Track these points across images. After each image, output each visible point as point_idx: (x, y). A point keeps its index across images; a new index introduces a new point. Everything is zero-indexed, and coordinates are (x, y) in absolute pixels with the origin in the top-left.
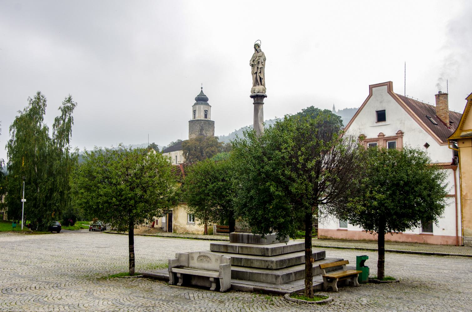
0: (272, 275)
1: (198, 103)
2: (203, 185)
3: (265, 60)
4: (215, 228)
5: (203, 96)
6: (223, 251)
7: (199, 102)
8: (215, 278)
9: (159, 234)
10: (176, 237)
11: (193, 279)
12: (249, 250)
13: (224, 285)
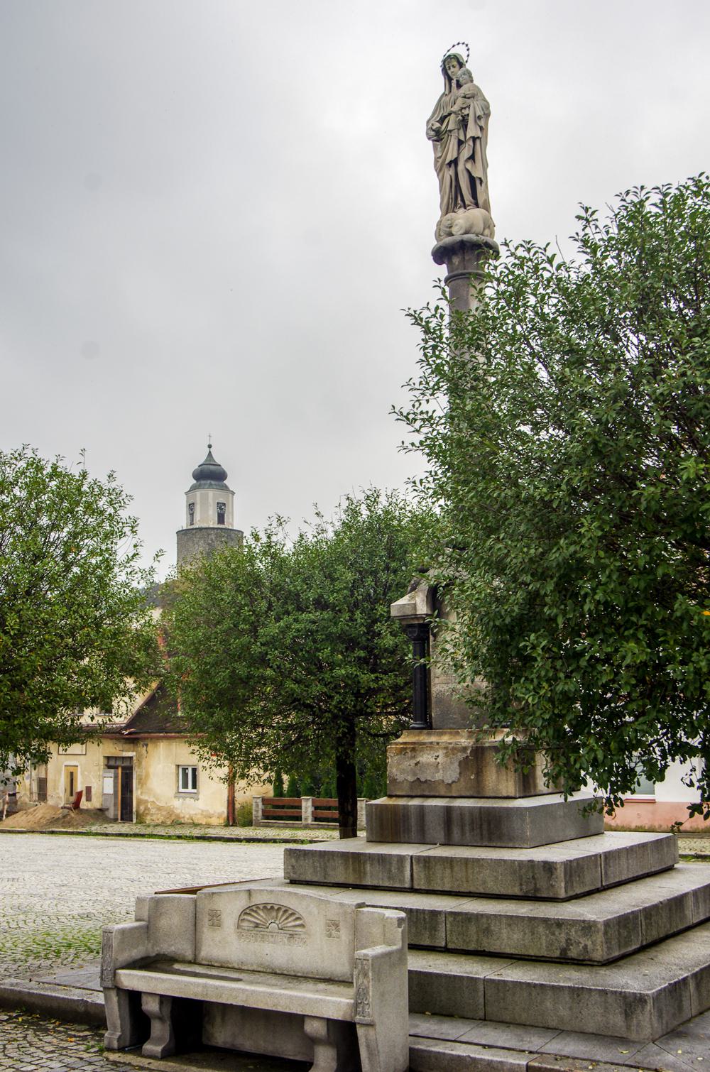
0: (604, 993)
1: (200, 485)
2: (241, 626)
3: (487, 115)
4: (257, 806)
5: (212, 467)
6: (341, 880)
7: (203, 482)
8: (329, 1021)
9: (94, 829)
10: (143, 836)
11: (218, 1020)
12: (459, 872)
13: (382, 1058)
